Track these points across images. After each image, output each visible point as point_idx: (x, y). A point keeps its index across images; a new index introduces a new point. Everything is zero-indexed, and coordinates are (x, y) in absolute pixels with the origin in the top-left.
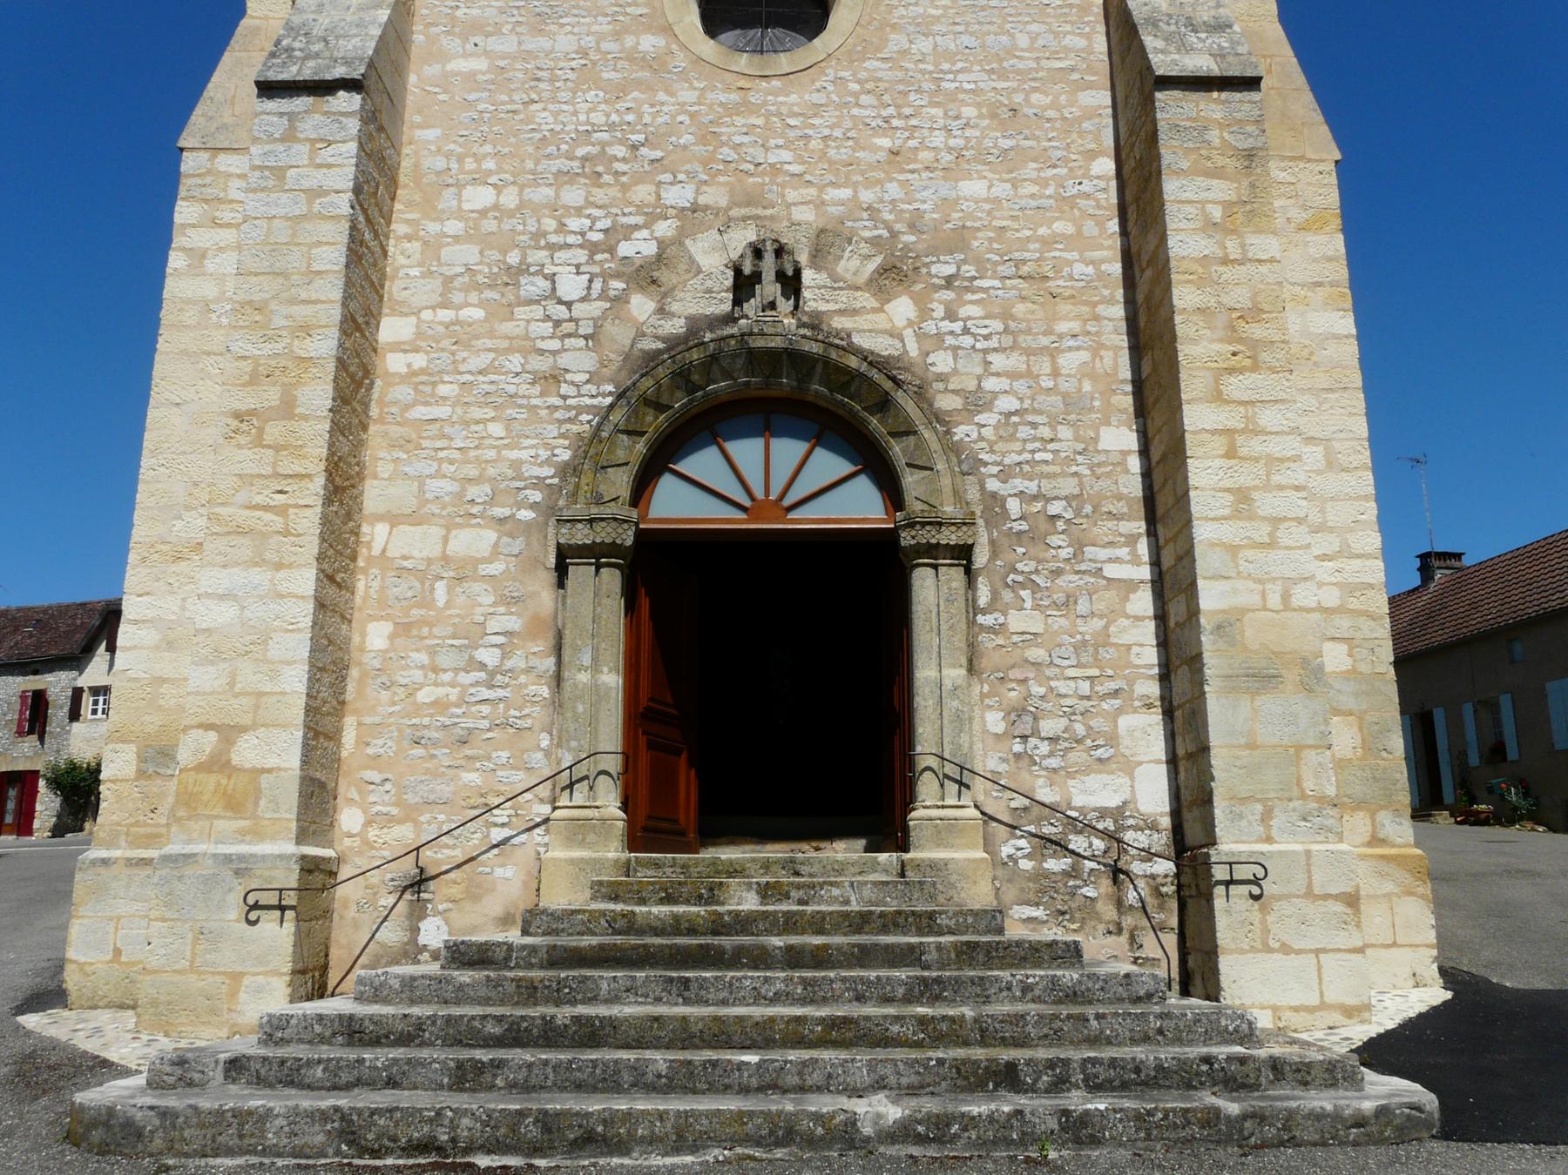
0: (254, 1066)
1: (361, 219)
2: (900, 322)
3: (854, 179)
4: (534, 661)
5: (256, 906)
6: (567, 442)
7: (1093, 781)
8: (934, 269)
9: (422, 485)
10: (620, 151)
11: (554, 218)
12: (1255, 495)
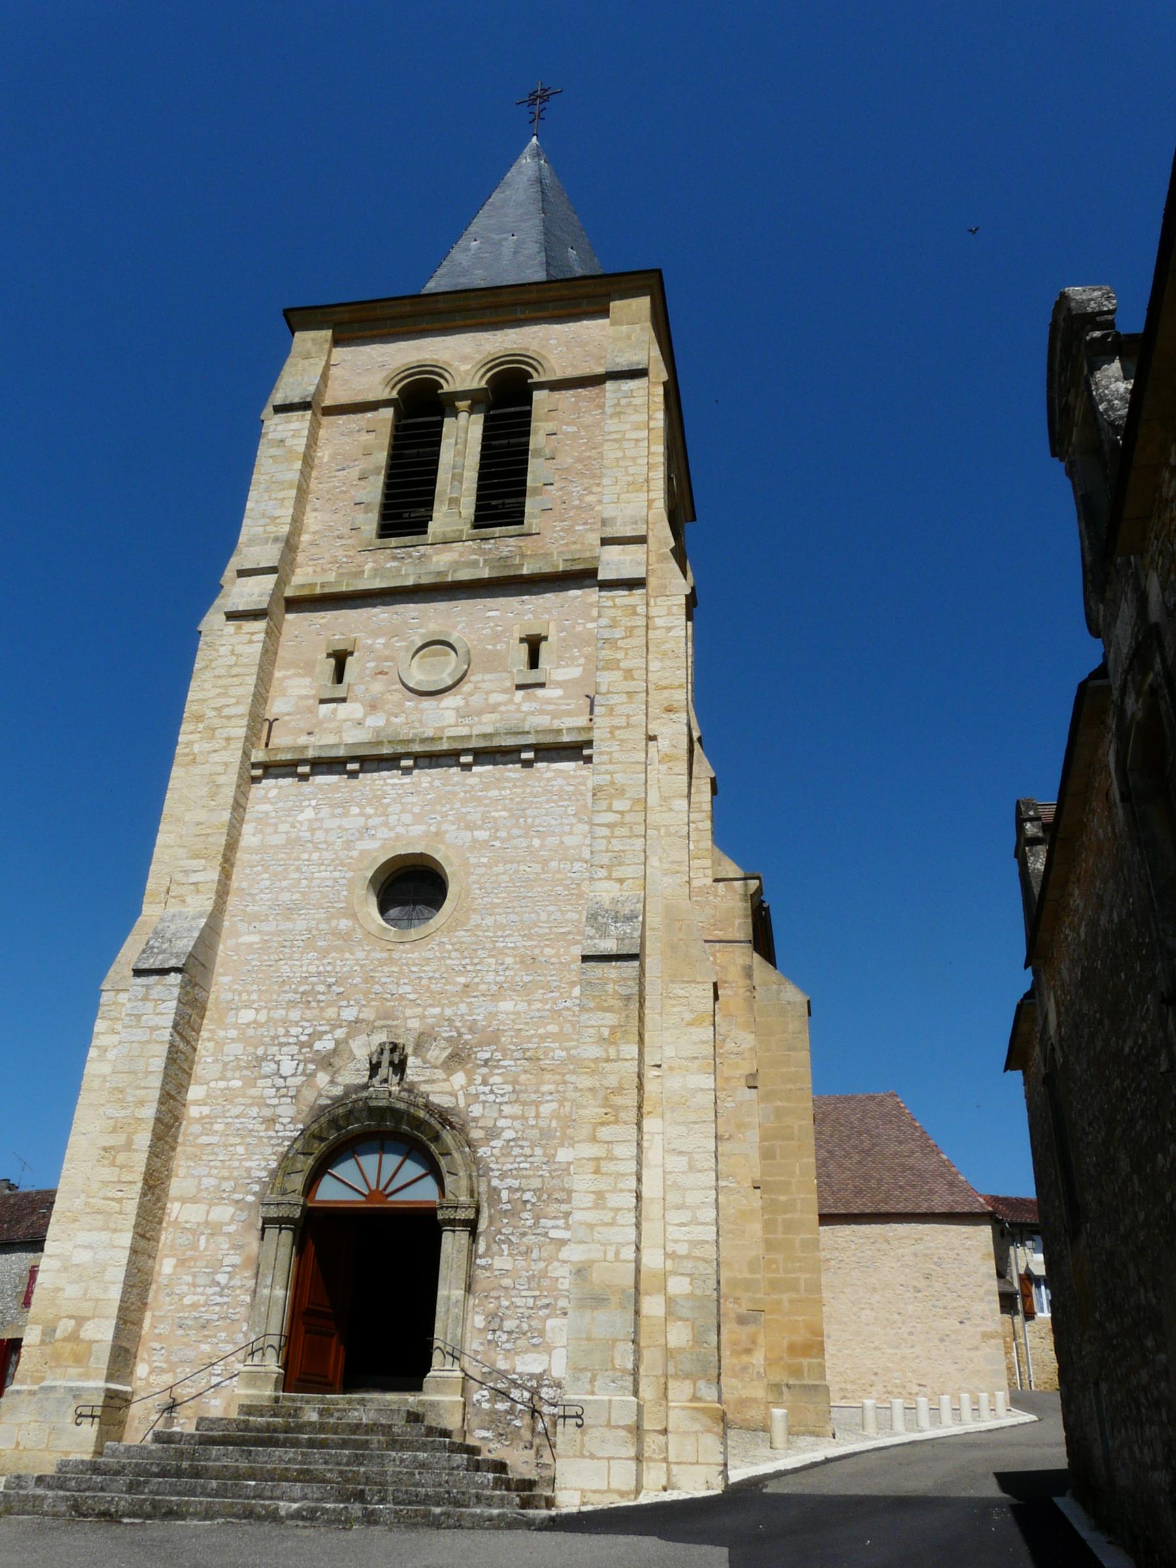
0: (48, 1479)
1: (178, 1039)
2: (457, 1087)
3: (443, 1002)
4: (245, 1282)
5: (80, 1416)
6: (275, 1157)
7: (529, 1357)
8: (479, 1055)
9: (200, 1180)
10: (321, 988)
11: (284, 1027)
12: (607, 1195)
